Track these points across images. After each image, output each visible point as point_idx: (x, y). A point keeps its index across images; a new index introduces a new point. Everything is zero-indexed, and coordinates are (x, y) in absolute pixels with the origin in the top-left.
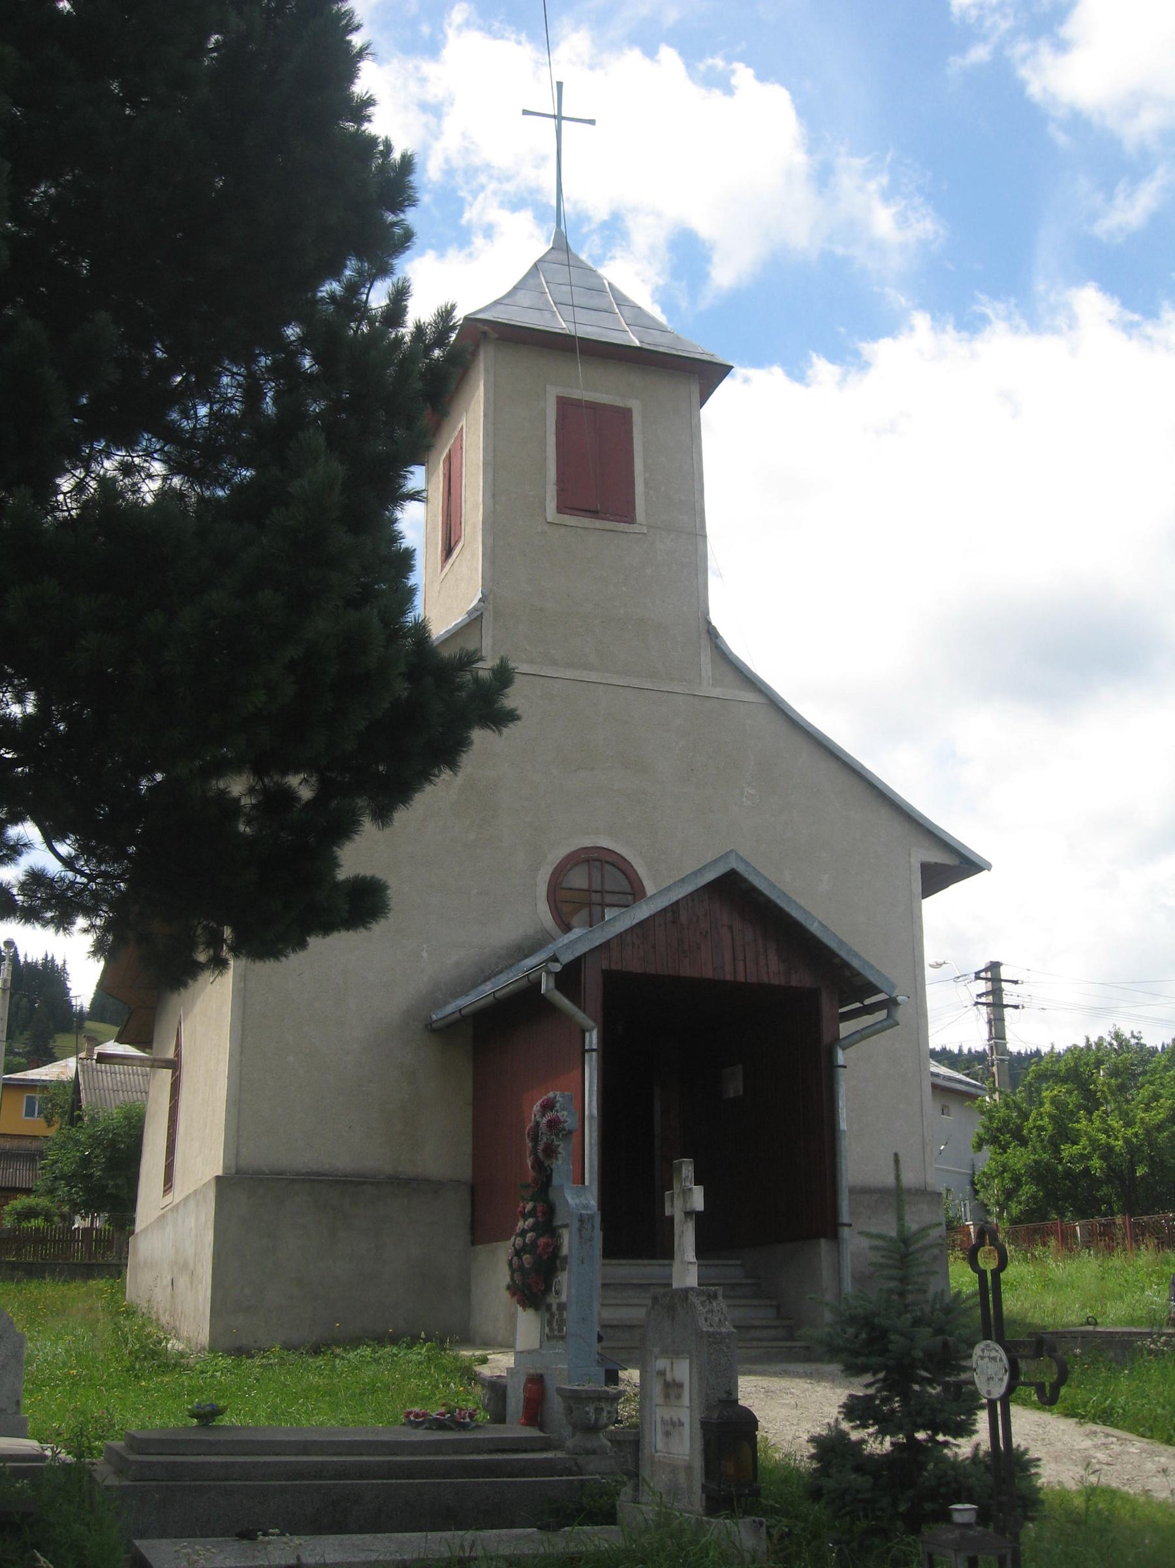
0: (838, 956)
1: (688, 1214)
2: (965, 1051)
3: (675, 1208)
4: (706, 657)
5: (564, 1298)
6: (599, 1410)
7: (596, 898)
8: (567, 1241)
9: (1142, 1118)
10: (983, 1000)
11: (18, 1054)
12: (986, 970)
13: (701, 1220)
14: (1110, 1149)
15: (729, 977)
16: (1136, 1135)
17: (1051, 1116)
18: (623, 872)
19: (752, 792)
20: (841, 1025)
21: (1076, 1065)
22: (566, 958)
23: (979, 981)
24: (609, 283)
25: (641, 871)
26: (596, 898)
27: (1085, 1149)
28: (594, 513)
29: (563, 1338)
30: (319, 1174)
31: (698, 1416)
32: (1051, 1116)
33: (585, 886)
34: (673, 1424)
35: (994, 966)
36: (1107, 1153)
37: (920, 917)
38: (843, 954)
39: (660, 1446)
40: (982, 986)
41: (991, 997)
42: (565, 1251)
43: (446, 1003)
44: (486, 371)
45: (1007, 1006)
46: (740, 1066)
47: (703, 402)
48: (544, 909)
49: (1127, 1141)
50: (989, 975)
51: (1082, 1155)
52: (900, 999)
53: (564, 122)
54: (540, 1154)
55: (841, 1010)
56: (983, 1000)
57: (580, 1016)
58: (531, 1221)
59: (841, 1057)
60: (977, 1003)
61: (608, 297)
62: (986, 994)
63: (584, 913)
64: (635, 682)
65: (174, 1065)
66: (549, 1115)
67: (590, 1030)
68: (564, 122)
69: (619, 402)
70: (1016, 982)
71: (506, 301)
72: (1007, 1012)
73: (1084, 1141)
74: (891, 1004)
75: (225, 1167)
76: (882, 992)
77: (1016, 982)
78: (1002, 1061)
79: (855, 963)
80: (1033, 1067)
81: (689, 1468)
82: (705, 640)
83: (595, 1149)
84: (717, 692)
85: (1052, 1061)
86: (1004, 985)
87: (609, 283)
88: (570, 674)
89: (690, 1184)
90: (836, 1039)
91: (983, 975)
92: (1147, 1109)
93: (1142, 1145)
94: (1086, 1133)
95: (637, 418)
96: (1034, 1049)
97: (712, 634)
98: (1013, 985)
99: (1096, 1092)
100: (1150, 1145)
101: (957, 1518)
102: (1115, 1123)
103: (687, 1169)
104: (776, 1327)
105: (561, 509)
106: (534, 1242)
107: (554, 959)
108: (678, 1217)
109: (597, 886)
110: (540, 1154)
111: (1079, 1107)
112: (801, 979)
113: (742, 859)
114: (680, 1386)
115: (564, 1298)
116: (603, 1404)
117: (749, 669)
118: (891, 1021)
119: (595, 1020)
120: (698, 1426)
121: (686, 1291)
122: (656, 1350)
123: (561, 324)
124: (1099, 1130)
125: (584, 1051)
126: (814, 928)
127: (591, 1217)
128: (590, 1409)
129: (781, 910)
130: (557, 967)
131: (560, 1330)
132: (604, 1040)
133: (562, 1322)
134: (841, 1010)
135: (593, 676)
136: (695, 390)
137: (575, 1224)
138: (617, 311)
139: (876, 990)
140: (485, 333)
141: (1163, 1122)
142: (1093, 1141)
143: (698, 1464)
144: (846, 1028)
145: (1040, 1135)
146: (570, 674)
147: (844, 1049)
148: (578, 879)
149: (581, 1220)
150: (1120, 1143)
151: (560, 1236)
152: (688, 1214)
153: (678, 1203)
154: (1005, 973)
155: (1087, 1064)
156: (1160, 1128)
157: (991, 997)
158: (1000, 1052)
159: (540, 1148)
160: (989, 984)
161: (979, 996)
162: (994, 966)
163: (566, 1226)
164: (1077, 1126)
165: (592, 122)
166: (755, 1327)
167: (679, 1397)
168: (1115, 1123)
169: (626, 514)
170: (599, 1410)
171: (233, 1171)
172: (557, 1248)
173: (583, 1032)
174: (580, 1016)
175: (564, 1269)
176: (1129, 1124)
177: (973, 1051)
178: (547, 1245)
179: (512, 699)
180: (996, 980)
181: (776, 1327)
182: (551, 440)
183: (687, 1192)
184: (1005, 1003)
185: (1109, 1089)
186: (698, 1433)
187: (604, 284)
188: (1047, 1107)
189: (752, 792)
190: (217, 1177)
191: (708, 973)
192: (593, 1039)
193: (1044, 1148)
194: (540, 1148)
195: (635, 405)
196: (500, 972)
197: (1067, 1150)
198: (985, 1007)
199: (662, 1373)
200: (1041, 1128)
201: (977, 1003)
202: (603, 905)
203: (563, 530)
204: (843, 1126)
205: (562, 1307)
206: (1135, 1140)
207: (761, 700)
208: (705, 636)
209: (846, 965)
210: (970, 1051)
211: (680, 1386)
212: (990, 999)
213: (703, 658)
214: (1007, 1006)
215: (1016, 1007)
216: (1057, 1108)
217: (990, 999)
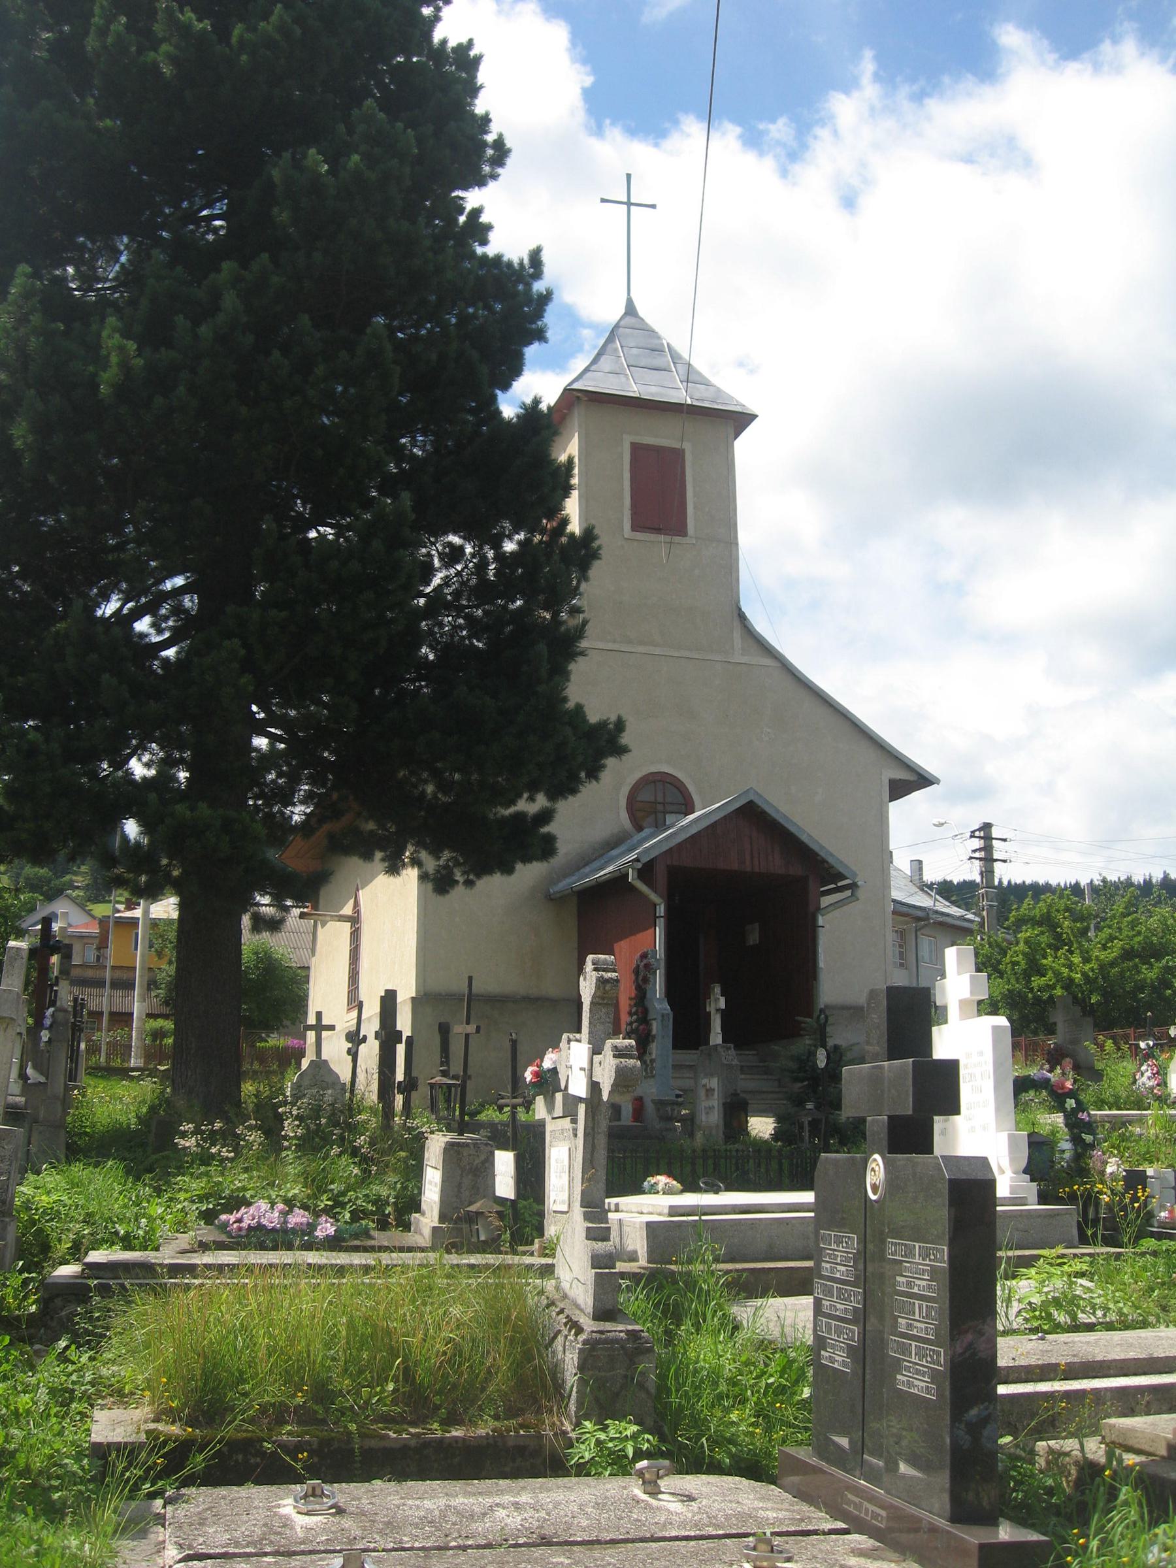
0: (818, 855)
1: (717, 1010)
2: (1005, 883)
3: (711, 1008)
4: (737, 634)
5: (654, 1056)
6: (673, 1110)
7: (660, 807)
8: (655, 1027)
9: (1096, 956)
10: (977, 855)
11: (78, 888)
12: (979, 830)
13: (724, 1014)
14: (1072, 980)
15: (749, 869)
16: (1092, 970)
17: (1024, 954)
18: (681, 792)
19: (769, 730)
20: (822, 899)
21: (1048, 912)
22: (645, 860)
23: (973, 839)
24: (668, 344)
25: (691, 788)
26: (660, 807)
27: (1050, 980)
28: (658, 530)
29: (653, 1077)
30: (455, 995)
31: (721, 1102)
32: (1024, 954)
33: (652, 799)
34: (710, 1108)
35: (987, 827)
36: (1069, 984)
37: (887, 818)
38: (822, 854)
39: (704, 1119)
40: (977, 843)
41: (983, 853)
42: (654, 1032)
43: (559, 881)
44: (580, 426)
45: (997, 860)
46: (757, 925)
47: (737, 435)
48: (624, 816)
49: (1084, 974)
50: (982, 834)
51: (1048, 985)
52: (859, 883)
53: (632, 208)
54: (640, 982)
55: (822, 889)
56: (977, 855)
57: (654, 897)
58: (635, 1017)
59: (821, 920)
60: (971, 858)
61: (666, 356)
62: (980, 850)
63: (651, 819)
64: (687, 654)
65: (355, 920)
66: (645, 961)
67: (660, 905)
68: (632, 208)
69: (675, 445)
70: (1005, 840)
71: (593, 368)
72: (997, 865)
73: (1050, 974)
74: (853, 886)
75: (417, 991)
76: (847, 878)
77: (1005, 840)
78: (991, 906)
79: (830, 860)
80: (1014, 913)
81: (717, 1126)
82: (737, 623)
83: (663, 978)
84: (745, 660)
85: (1029, 909)
86: (994, 842)
87: (668, 344)
88: (641, 649)
89: (719, 996)
90: (818, 909)
91: (977, 834)
92: (1104, 947)
93: (1097, 978)
94: (1051, 968)
95: (689, 458)
96: (1073, 882)
97: (742, 617)
98: (1003, 843)
99: (1062, 933)
100: (1103, 978)
101: (808, 1107)
102: (1076, 959)
103: (717, 989)
104: (779, 1092)
105: (634, 528)
106: (637, 1028)
107: (637, 860)
108: (713, 1012)
109: (660, 799)
110: (640, 982)
111: (1050, 946)
112: (796, 870)
113: (757, 793)
114: (714, 1090)
115: (654, 1056)
116: (675, 1107)
117: (768, 643)
118: (854, 898)
119: (661, 897)
120: (721, 1105)
121: (716, 1046)
122: (702, 1075)
123: (633, 389)
124: (1064, 965)
125: (656, 917)
126: (804, 838)
127: (668, 1014)
128: (669, 1109)
129: (783, 826)
130: (639, 865)
131: (652, 1072)
132: (669, 909)
133: (653, 1069)
134: (822, 889)
135: (657, 651)
136: (731, 431)
137: (660, 1018)
138: (674, 369)
139: (842, 877)
140: (578, 397)
141: (1116, 959)
142: (1057, 974)
143: (721, 1123)
144: (825, 901)
145: (1013, 969)
146: (641, 649)
147: (823, 915)
148: (646, 796)
149: (663, 1016)
150: (1079, 976)
151: (651, 1025)
152: (717, 1010)
153: (713, 1005)
154: (995, 833)
155: (1058, 911)
156: (1112, 964)
157: (983, 853)
158: (990, 898)
159: (640, 978)
160: (982, 841)
161: (974, 851)
162: (987, 827)
163: (655, 1019)
164: (1044, 962)
165: (653, 206)
166: (764, 1092)
167: (713, 1095)
168: (1076, 959)
169: (681, 530)
170: (673, 1110)
171: (422, 993)
172: (650, 1031)
173: (655, 905)
174: (654, 897)
175: (653, 1041)
176: (1086, 960)
177: (1013, 883)
178: (644, 1029)
179: (625, 739)
180: (988, 838)
181: (779, 1092)
182: (627, 475)
183: (717, 1000)
184: (995, 857)
185: (1072, 932)
186: (722, 1109)
187: (663, 344)
188: (1022, 946)
189: (769, 730)
190: (412, 998)
191: (735, 866)
192: (661, 910)
193: (1017, 980)
194: (640, 978)
195: (687, 446)
196: (595, 860)
197: (1037, 982)
198: (978, 861)
199: (705, 1086)
200: (1015, 964)
201: (971, 858)
202: (665, 813)
203: (636, 543)
204: (821, 964)
205: (652, 1061)
206: (1091, 974)
207: (779, 665)
208: (736, 618)
209: (824, 861)
210: (1009, 882)
211: (714, 1090)
212: (981, 854)
213: (735, 634)
214: (997, 860)
215: (1005, 861)
216: (1030, 947)
217: (981, 854)
